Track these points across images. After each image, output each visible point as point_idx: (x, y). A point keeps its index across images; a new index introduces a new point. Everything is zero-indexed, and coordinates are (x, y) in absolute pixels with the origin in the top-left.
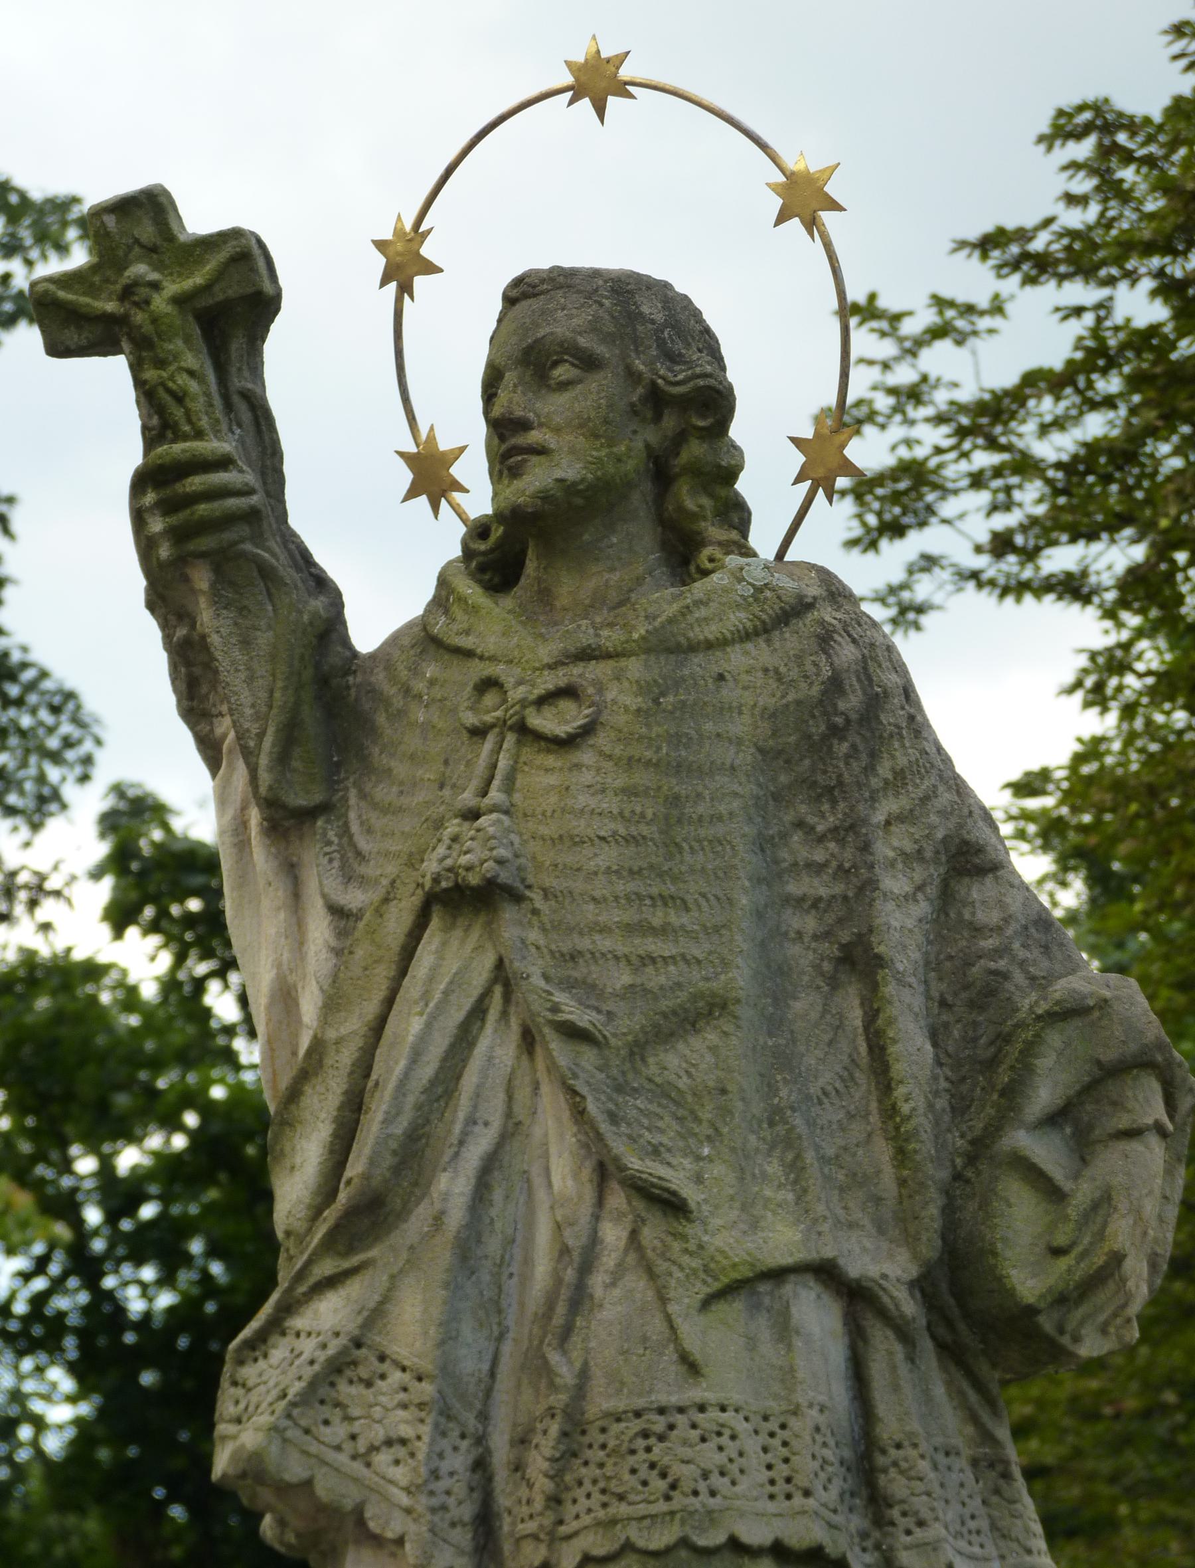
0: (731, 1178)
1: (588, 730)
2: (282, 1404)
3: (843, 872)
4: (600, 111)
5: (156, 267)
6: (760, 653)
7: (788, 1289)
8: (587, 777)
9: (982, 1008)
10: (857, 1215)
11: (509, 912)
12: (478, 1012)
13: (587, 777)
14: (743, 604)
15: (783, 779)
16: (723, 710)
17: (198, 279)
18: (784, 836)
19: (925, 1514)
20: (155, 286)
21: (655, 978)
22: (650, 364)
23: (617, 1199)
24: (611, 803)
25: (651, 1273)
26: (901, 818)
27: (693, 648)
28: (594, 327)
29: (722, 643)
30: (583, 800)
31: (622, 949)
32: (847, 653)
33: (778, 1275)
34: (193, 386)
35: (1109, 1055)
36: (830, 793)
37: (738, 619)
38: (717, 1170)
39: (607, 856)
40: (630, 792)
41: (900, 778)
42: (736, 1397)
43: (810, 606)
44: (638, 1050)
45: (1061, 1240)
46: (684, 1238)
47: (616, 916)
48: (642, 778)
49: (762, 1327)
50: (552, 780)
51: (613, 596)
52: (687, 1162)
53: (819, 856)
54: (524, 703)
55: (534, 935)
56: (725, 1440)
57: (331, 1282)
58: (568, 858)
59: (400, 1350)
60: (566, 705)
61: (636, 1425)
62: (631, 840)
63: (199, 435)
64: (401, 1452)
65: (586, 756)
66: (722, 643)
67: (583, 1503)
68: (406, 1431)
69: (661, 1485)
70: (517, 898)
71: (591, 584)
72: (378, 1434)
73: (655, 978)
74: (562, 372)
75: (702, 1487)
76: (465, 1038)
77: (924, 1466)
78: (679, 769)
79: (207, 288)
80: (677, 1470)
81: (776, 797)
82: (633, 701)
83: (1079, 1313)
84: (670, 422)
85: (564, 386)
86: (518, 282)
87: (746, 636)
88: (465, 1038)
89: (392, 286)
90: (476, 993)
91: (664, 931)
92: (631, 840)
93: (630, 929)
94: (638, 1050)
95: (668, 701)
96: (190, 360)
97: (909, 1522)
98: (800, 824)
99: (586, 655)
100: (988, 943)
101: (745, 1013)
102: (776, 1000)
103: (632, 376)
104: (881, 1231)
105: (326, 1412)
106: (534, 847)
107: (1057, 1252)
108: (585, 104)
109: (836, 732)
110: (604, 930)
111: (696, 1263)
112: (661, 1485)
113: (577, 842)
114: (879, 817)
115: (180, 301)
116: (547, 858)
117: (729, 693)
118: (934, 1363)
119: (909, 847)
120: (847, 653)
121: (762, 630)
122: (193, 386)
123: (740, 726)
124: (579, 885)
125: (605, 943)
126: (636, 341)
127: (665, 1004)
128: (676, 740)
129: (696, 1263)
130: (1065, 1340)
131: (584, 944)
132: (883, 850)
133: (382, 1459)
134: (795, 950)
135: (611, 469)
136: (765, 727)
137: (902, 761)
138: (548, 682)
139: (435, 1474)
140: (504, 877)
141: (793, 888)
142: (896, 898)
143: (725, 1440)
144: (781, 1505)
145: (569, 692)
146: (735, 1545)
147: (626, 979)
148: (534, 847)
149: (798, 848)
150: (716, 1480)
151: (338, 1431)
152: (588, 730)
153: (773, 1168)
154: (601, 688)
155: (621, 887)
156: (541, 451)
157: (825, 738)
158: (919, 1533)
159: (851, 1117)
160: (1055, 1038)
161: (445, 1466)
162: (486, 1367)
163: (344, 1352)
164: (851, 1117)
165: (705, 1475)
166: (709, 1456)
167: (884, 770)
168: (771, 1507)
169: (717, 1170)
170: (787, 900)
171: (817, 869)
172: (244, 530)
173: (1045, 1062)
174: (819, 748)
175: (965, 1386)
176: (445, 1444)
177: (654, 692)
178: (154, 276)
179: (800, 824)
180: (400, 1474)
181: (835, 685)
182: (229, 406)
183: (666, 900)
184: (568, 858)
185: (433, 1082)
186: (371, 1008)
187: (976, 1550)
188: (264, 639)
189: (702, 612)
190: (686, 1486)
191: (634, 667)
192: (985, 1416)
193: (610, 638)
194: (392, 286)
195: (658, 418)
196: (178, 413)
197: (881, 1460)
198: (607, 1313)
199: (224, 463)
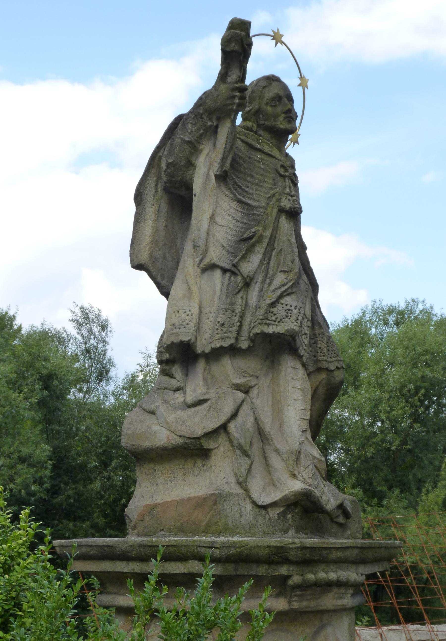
57: (289, 294)
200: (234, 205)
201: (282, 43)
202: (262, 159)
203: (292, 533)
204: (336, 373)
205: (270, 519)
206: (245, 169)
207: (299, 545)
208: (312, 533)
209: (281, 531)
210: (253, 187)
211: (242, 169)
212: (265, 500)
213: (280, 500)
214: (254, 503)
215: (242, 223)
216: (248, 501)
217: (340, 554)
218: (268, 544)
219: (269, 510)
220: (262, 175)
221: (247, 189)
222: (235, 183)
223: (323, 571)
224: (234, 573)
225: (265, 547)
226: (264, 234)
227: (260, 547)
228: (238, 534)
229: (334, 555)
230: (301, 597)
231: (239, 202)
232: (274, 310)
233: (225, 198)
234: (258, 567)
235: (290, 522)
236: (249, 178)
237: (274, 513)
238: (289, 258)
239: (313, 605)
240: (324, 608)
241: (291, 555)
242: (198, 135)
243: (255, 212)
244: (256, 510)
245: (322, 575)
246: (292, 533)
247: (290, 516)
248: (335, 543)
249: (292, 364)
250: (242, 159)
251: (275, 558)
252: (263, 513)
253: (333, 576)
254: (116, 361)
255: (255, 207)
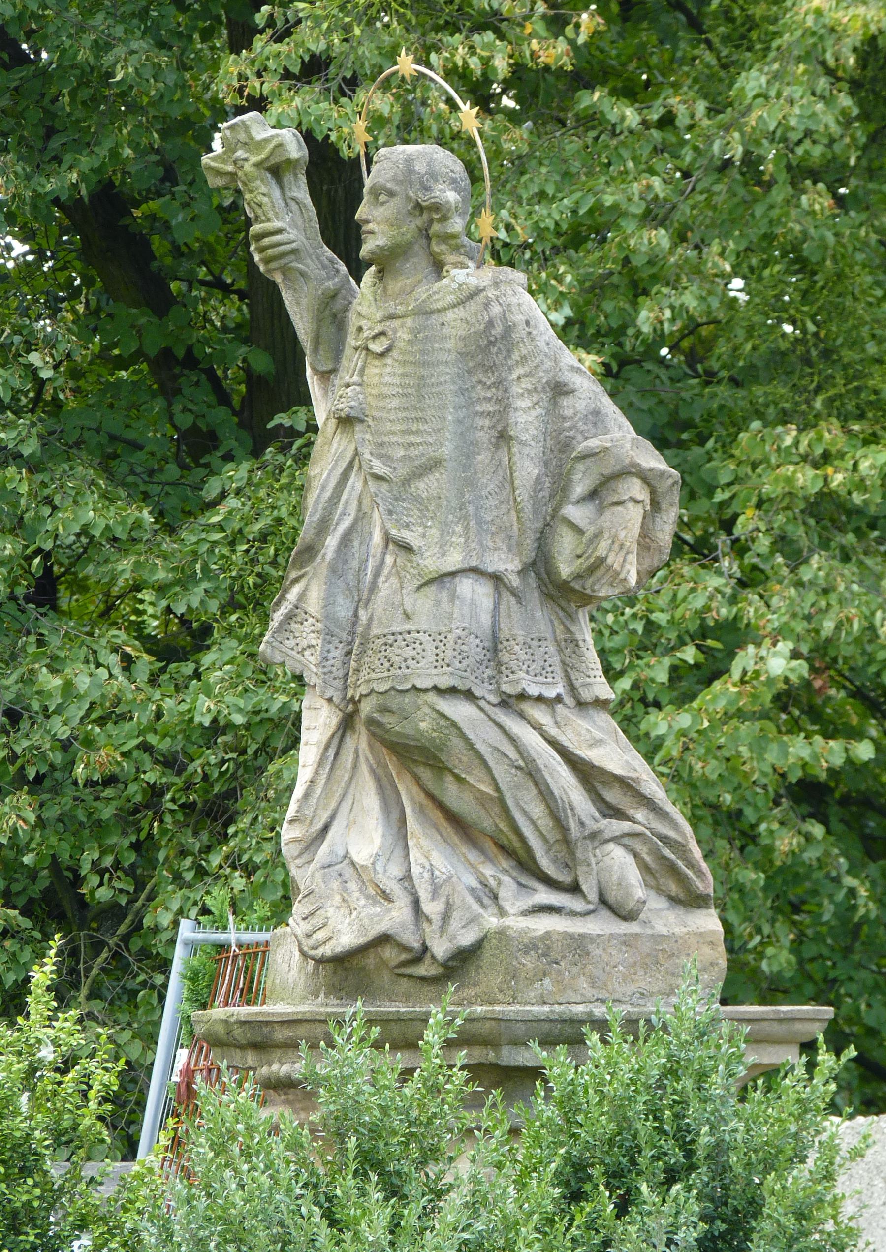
0: (438, 534)
1: (389, 350)
3: (498, 401)
5: (247, 151)
6: (460, 312)
7: (457, 579)
8: (389, 369)
9: (564, 452)
10: (500, 544)
11: (358, 427)
13: (389, 369)
14: (454, 292)
15: (471, 364)
16: (444, 338)
17: (263, 156)
18: (473, 387)
19: (515, 668)
20: (246, 160)
21: (414, 452)
22: (416, 193)
23: (391, 547)
24: (397, 380)
26: (525, 376)
27: (432, 312)
28: (394, 179)
29: (444, 309)
30: (387, 379)
31: (400, 441)
32: (496, 309)
33: (453, 574)
34: (265, 200)
35: (607, 472)
36: (491, 368)
37: (451, 299)
38: (433, 531)
39: (395, 403)
40: (404, 375)
41: (524, 359)
42: (424, 627)
43: (483, 290)
44: (406, 482)
45: (579, 552)
46: (411, 561)
47: (398, 427)
48: (409, 369)
49: (444, 596)
50: (377, 371)
51: (408, 289)
52: (420, 529)
53: (489, 395)
54: (367, 339)
55: (368, 436)
56: (417, 645)
59: (311, 610)
60: (383, 338)
61: (383, 640)
62: (404, 395)
63: (269, 220)
64: (312, 650)
65: (389, 361)
66: (444, 309)
68: (314, 642)
69: (387, 665)
70: (362, 421)
72: (304, 643)
73: (414, 452)
75: (403, 665)
77: (517, 648)
78: (425, 364)
79: (267, 159)
80: (395, 659)
81: (469, 372)
82: (406, 336)
83: (590, 581)
84: (425, 216)
85: (383, 204)
87: (454, 306)
90: (348, 460)
91: (417, 432)
92: (404, 395)
93: (404, 432)
94: (406, 482)
95: (421, 335)
96: (263, 189)
97: (508, 672)
98: (480, 382)
99: (391, 317)
100: (567, 424)
101: (450, 465)
102: (468, 457)
103: (409, 199)
104: (510, 550)
105: (287, 634)
106: (370, 399)
107: (579, 556)
109: (491, 343)
110: (394, 433)
111: (415, 572)
112: (387, 665)
114: (514, 376)
115: (257, 165)
116: (373, 404)
117: (446, 331)
118: (538, 602)
119: (530, 387)
120: (496, 309)
121: (461, 303)
122: (265, 200)
123: (450, 345)
124: (385, 415)
125: (394, 439)
126: (411, 183)
127: (417, 463)
128: (423, 352)
129: (415, 572)
130: (588, 591)
131: (386, 439)
132: (516, 389)
133: (307, 653)
134: (482, 433)
135: (399, 239)
136: (461, 344)
137: (524, 351)
138: (378, 328)
139: (326, 659)
140: (353, 413)
141: (479, 408)
142: (523, 410)
143: (417, 645)
144: (439, 670)
145: (383, 333)
146: (415, 688)
147: (402, 453)
148: (370, 399)
149: (480, 391)
150: (410, 662)
151: (291, 643)
152: (389, 350)
153: (459, 528)
154: (395, 331)
155: (401, 415)
157: (487, 346)
158: (511, 676)
159: (501, 502)
160: (581, 467)
161: (331, 655)
162: (351, 613)
163: (291, 611)
164: (501, 502)
165: (405, 660)
166: (409, 652)
167: (516, 356)
168: (434, 671)
169: (433, 531)
170: (476, 414)
171: (486, 399)
172: (293, 257)
173: (577, 477)
174: (485, 350)
175: (558, 609)
176: (331, 646)
177: (415, 332)
178: (245, 156)
179: (480, 382)
180: (312, 659)
181: (491, 324)
182: (287, 205)
183: (418, 419)
184: (381, 404)
185: (330, 498)
187: (550, 680)
188: (304, 301)
189: (437, 297)
190: (396, 666)
191: (409, 321)
192: (567, 623)
193: (400, 310)
195: (421, 214)
196: (259, 211)
197: (500, 647)
198: (381, 594)
199: (279, 231)
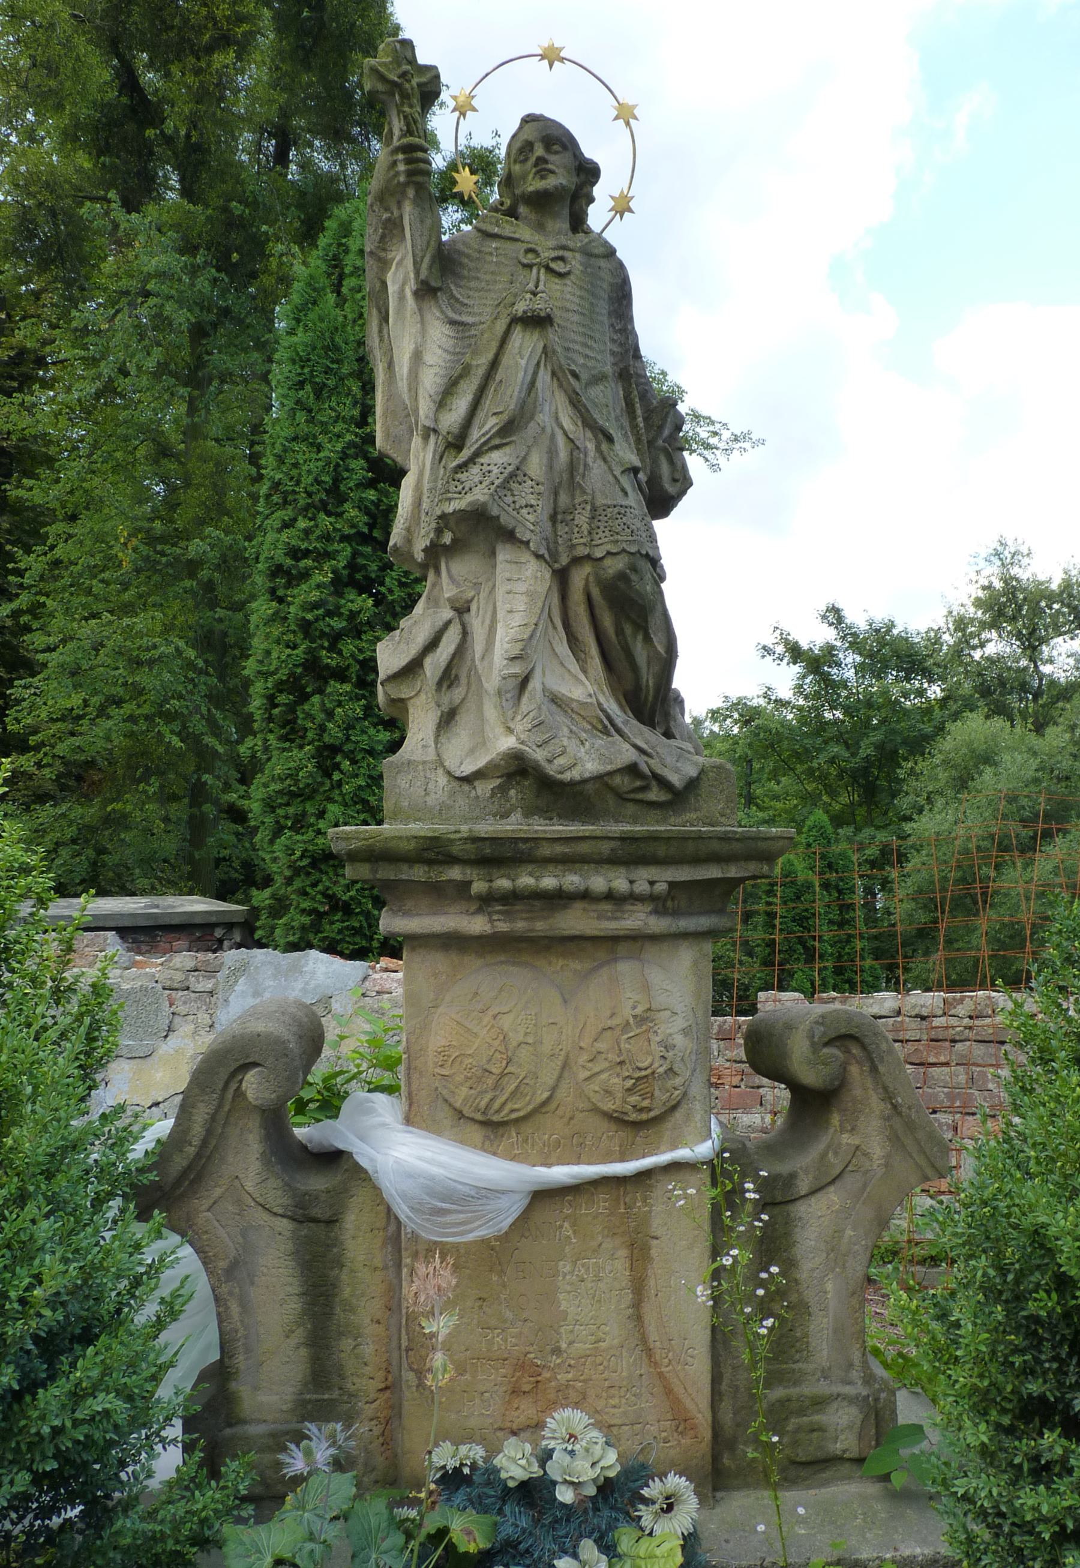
2: (493, 487)
4: (551, 66)
12: (538, 364)
24: (577, 300)
25: (605, 460)
47: (579, 339)
57: (497, 447)
58: (564, 315)
61: (616, 510)
67: (601, 534)
68: (533, 502)
71: (558, 226)
74: (556, 147)
76: (535, 373)
85: (556, 153)
86: (528, 116)
88: (535, 373)
89: (457, 114)
105: (506, 492)
108: (546, 62)
113: (568, 310)
124: (569, 325)
156: (552, 172)
180: (531, 518)
186: (490, 356)
194: (457, 114)
200: (447, 330)
201: (562, 60)
202: (496, 249)
203: (516, 817)
204: (608, 562)
205: (477, 797)
206: (469, 270)
207: (465, 835)
208: (560, 817)
209: (495, 816)
210: (476, 294)
211: (465, 272)
212: (468, 768)
213: (486, 767)
214: (449, 773)
215: (454, 354)
216: (440, 771)
217: (559, 849)
218: (413, 833)
219: (476, 783)
220: (493, 273)
221: (466, 301)
222: (452, 296)
223: (531, 875)
224: (371, 877)
225: (408, 839)
226: (474, 363)
227: (400, 838)
228: (419, 820)
229: (546, 851)
230: (508, 915)
231: (452, 323)
232: (462, 476)
233: (437, 323)
234: (410, 867)
235: (514, 801)
236: (472, 284)
237: (484, 788)
238: (509, 393)
239: (540, 927)
240: (566, 933)
241: (455, 850)
242: (378, 238)
243: (473, 332)
244: (455, 784)
245: (526, 881)
246: (516, 817)
247: (512, 792)
248: (545, 832)
249: (508, 557)
250: (468, 256)
251: (431, 855)
252: (466, 787)
253: (549, 882)
254: (880, 616)
255: (473, 325)
